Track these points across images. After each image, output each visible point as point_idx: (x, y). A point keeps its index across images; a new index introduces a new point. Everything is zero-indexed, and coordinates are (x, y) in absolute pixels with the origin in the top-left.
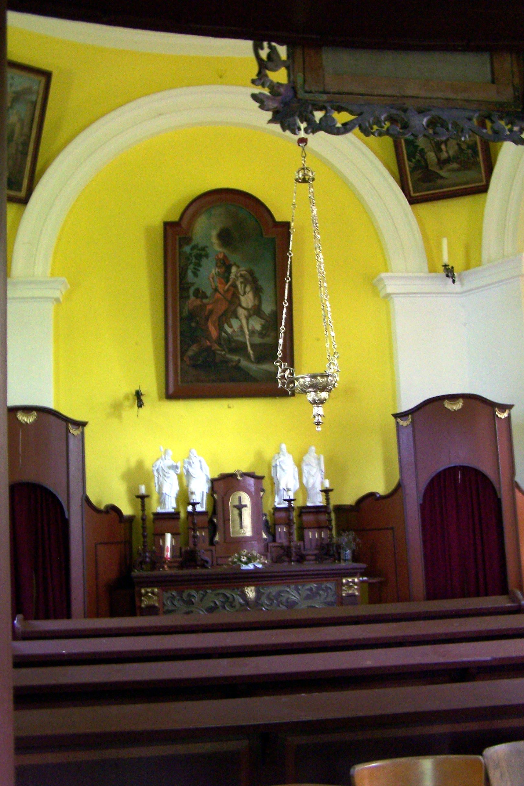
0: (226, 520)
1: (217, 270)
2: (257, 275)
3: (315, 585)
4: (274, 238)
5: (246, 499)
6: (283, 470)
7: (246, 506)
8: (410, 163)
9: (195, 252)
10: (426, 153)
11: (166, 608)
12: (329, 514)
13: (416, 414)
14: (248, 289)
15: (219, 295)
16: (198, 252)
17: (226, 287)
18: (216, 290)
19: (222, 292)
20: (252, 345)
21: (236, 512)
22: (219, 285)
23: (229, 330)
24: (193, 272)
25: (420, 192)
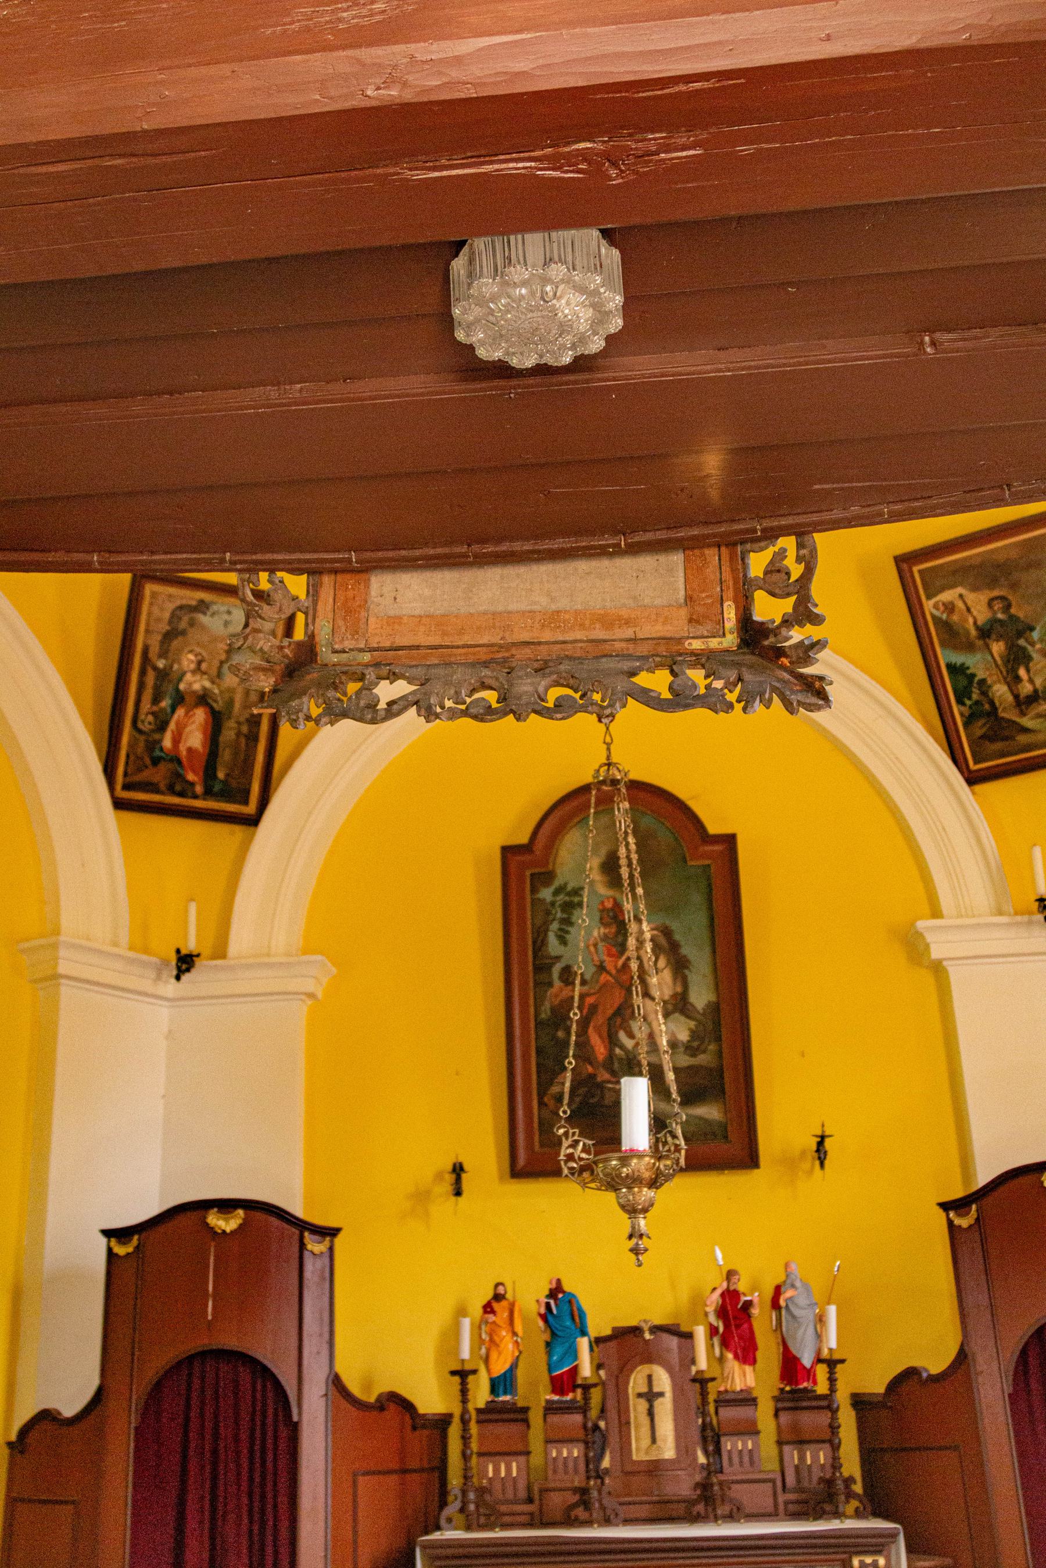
1: (602, 930)
2: (677, 937)
4: (709, 866)
5: (663, 1381)
6: (794, 1317)
7: (661, 1394)
8: (962, 708)
9: (561, 898)
10: (990, 687)
12: (834, 1411)
13: (989, 1200)
14: (662, 963)
16: (567, 898)
17: (620, 962)
18: (601, 968)
19: (614, 972)
20: (676, 1070)
21: (642, 1405)
23: (629, 1043)
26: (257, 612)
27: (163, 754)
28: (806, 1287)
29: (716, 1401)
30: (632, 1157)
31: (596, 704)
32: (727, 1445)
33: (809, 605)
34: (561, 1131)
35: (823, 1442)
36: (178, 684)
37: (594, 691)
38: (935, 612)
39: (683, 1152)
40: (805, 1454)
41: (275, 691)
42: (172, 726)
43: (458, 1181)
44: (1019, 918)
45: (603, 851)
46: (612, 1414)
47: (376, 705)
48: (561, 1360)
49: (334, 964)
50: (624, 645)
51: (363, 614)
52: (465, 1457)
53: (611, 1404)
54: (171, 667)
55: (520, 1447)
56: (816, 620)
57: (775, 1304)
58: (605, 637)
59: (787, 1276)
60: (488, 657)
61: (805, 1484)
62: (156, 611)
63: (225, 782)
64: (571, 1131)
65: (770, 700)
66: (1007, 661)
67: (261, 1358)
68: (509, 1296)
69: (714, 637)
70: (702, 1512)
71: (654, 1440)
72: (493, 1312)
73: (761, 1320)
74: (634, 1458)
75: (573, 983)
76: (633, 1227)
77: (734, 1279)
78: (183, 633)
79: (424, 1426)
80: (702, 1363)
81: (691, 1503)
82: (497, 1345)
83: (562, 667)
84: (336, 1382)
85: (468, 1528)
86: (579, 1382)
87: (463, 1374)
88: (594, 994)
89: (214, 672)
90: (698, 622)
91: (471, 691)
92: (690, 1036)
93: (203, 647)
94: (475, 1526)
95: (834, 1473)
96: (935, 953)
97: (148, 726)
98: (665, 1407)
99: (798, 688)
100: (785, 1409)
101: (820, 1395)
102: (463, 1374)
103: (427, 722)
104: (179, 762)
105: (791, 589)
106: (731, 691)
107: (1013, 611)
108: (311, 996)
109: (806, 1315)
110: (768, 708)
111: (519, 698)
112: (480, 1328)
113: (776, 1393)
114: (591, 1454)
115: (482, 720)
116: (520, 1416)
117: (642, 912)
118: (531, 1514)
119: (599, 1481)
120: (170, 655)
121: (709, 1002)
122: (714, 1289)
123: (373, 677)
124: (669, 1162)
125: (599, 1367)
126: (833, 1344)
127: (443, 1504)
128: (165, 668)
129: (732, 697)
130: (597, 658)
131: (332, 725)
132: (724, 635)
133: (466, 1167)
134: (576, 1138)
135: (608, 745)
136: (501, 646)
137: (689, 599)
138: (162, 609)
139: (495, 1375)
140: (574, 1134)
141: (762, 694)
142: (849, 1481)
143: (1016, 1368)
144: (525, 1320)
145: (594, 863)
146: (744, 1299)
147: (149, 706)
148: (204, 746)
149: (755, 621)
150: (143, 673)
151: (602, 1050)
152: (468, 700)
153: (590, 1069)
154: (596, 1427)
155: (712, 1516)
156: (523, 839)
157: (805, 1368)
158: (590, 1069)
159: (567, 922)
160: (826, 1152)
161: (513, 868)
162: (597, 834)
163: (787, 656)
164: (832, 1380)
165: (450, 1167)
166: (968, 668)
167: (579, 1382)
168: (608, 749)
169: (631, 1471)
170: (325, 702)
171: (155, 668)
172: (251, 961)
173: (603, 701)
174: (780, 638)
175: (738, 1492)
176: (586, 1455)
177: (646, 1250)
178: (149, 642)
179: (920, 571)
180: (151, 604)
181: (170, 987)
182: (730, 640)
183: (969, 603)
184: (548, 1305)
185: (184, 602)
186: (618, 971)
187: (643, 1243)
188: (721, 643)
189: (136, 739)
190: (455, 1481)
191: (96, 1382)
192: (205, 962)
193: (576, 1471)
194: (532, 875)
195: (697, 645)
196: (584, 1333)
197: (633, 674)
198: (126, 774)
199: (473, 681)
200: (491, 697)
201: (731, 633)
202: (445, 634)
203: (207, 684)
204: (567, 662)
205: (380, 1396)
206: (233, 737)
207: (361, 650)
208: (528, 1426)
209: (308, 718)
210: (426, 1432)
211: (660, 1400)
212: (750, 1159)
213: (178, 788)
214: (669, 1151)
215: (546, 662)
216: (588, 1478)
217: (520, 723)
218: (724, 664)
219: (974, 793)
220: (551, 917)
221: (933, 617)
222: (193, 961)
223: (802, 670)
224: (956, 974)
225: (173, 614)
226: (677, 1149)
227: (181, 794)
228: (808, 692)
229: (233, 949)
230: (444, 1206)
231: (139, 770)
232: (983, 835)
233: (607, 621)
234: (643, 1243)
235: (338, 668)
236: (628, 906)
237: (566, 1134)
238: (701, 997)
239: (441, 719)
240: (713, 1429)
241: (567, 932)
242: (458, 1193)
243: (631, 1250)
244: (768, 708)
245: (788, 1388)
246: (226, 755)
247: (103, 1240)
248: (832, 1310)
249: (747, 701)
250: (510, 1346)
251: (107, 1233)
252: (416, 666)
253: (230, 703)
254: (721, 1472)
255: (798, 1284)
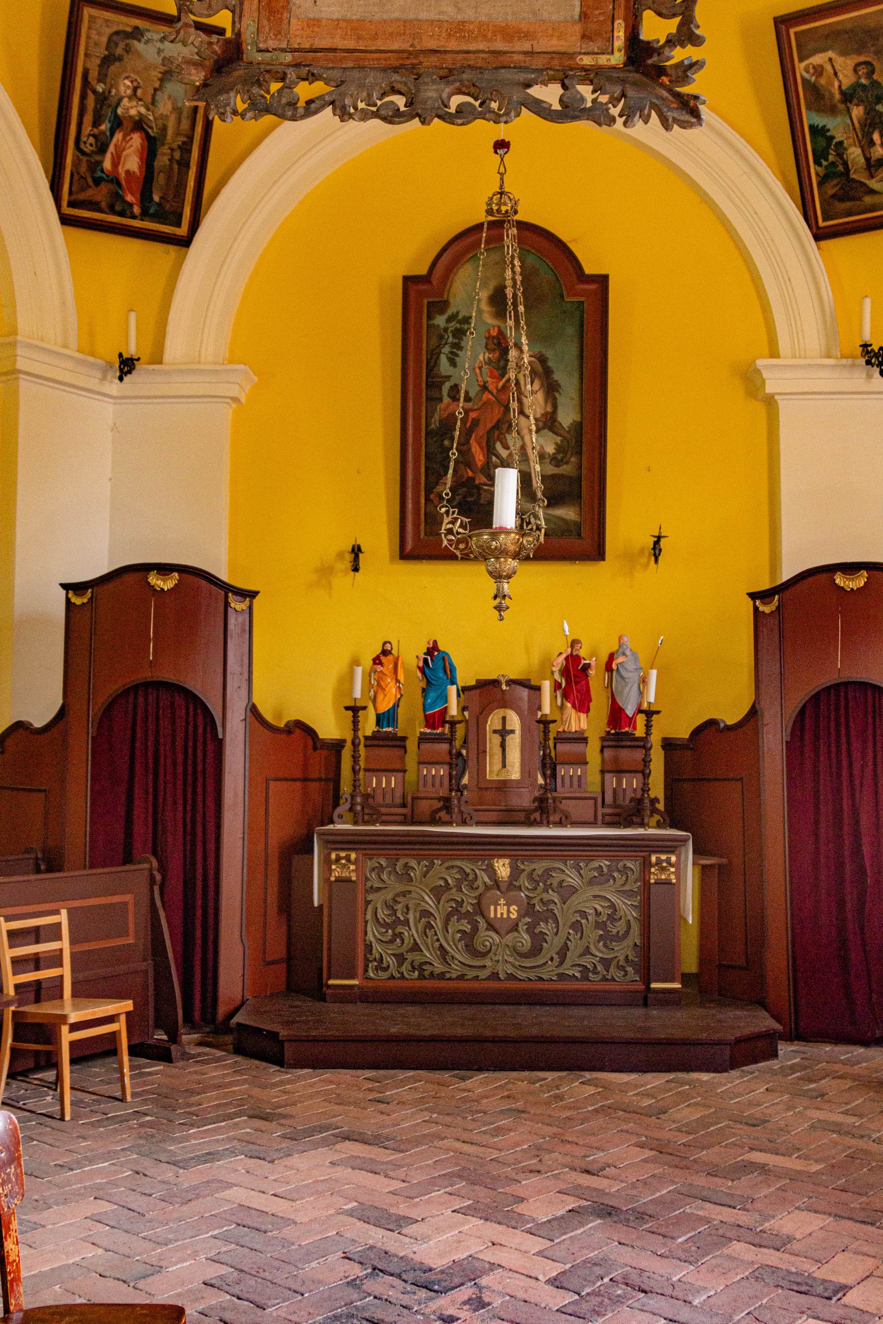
0: (481, 752)
2: (550, 364)
3: (607, 863)
5: (514, 721)
6: (622, 678)
7: (513, 732)
8: (819, 169)
9: (453, 325)
10: (846, 149)
11: (369, 884)
13: (787, 594)
15: (490, 396)
16: (458, 326)
17: (501, 384)
18: (484, 388)
19: (495, 391)
21: (497, 739)
22: (489, 379)
24: (448, 358)
25: (832, 219)
26: (188, 7)
27: (104, 175)
28: (636, 658)
29: (555, 739)
30: (501, 533)
31: (494, 112)
32: (561, 771)
33: (692, 26)
34: (443, 510)
35: (635, 772)
36: (116, 108)
37: (492, 100)
38: (806, 75)
39: (543, 531)
40: (622, 781)
41: (205, 85)
42: (112, 148)
43: (356, 559)
44: (844, 361)
45: (492, 285)
46: (473, 745)
47: (296, 103)
48: (434, 702)
49: (255, 374)
50: (521, 57)
51: (285, 15)
52: (355, 771)
53: (472, 737)
54: (110, 92)
55: (398, 767)
56: (696, 41)
57: (609, 668)
58: (505, 49)
59: (620, 646)
60: (397, 63)
61: (620, 802)
62: (94, 35)
63: (159, 204)
64: (451, 510)
65: (649, 116)
66: (863, 125)
67: (192, 689)
68: (394, 652)
69: (603, 54)
70: (538, 819)
71: (504, 766)
72: (381, 664)
73: (596, 680)
74: (488, 777)
75: (459, 400)
76: (498, 590)
77: (577, 647)
78: (120, 59)
79: (322, 748)
80: (546, 709)
81: (528, 812)
82: (383, 689)
83: (465, 76)
84: (253, 710)
85: (355, 823)
86: (448, 719)
87: (355, 710)
88: (476, 410)
89: (149, 99)
90: (590, 39)
91: (382, 95)
92: (555, 449)
93: (138, 73)
94: (360, 821)
95: (643, 795)
96: (769, 389)
97: (91, 148)
98: (514, 742)
99: (675, 106)
100: (609, 747)
101: (638, 738)
102: (355, 710)
103: (342, 121)
104: (119, 184)
105: (678, 10)
106: (615, 107)
107: (875, 77)
108: (235, 400)
109: (632, 677)
110: (646, 123)
111: (425, 103)
112: (370, 676)
113: (603, 735)
114: (454, 773)
115: (390, 122)
116: (398, 743)
117: (523, 328)
118: (405, 815)
119: (459, 793)
120: (108, 80)
121: (574, 421)
122: (561, 653)
123: (294, 76)
124: (531, 539)
125: (464, 709)
126: (652, 699)
127: (336, 804)
128: (104, 92)
129: (615, 111)
130: (496, 68)
131: (256, 120)
132: (612, 53)
133: (363, 549)
134: (455, 516)
135: (502, 175)
136: (410, 53)
137: (584, 16)
138: (99, 34)
139: (380, 712)
140: (453, 513)
141: (641, 110)
142: (654, 801)
143: (794, 726)
144: (407, 672)
145: (484, 295)
146: (583, 662)
147: (90, 128)
148: (140, 168)
149: (643, 41)
150: (83, 97)
151: (481, 458)
152: (379, 103)
153: (470, 473)
154: (459, 754)
155: (545, 822)
156: (423, 270)
157: (628, 716)
158: (470, 473)
159: (458, 346)
160: (660, 550)
161: (412, 293)
162: (488, 256)
163: (667, 75)
164: (648, 726)
165: (350, 549)
166: (828, 130)
167: (448, 719)
168: (502, 179)
169: (483, 786)
170: (250, 99)
171: (94, 92)
172: (183, 367)
173: (500, 109)
174: (662, 57)
175: (568, 806)
176: (450, 774)
177: (508, 608)
178: (89, 65)
179: (796, 33)
180: (89, 28)
181: (114, 387)
182: (618, 58)
183: (837, 67)
184: (425, 661)
185: (121, 28)
186: (499, 391)
187: (507, 602)
188: (609, 60)
189: (80, 160)
190: (346, 787)
191: (60, 702)
192: (144, 366)
193: (441, 785)
194: (429, 303)
195: (587, 61)
196: (453, 682)
197: (529, 86)
198: (70, 193)
199: (383, 85)
200: (400, 101)
201: (619, 50)
202: (359, 38)
203: (143, 110)
204: (468, 71)
205: (288, 722)
206: (168, 163)
207: (283, 50)
208: (406, 752)
209: (235, 112)
210: (325, 753)
211: (511, 735)
212: (598, 553)
213: (118, 208)
214: (531, 529)
215: (451, 71)
216: (451, 790)
217: (425, 127)
218: (610, 79)
219: (819, 248)
220: (444, 342)
221: (803, 78)
222: (134, 364)
223: (678, 89)
224: (783, 405)
225: (110, 40)
226: (539, 529)
227: (122, 214)
228: (683, 109)
229: (168, 356)
230: (344, 580)
231: (82, 189)
232: (823, 289)
233: (507, 32)
234: (507, 602)
235: (262, 66)
236: (511, 334)
237: (447, 512)
238: (567, 417)
239: (354, 119)
240: (551, 758)
241: (457, 355)
242: (356, 569)
243: (495, 608)
244: (646, 123)
245: (613, 731)
246: (160, 179)
247: (63, 592)
248: (654, 673)
249: (628, 116)
250: (394, 690)
251: (66, 587)
252: (333, 68)
253: (164, 129)
254: (556, 791)
255: (628, 653)
